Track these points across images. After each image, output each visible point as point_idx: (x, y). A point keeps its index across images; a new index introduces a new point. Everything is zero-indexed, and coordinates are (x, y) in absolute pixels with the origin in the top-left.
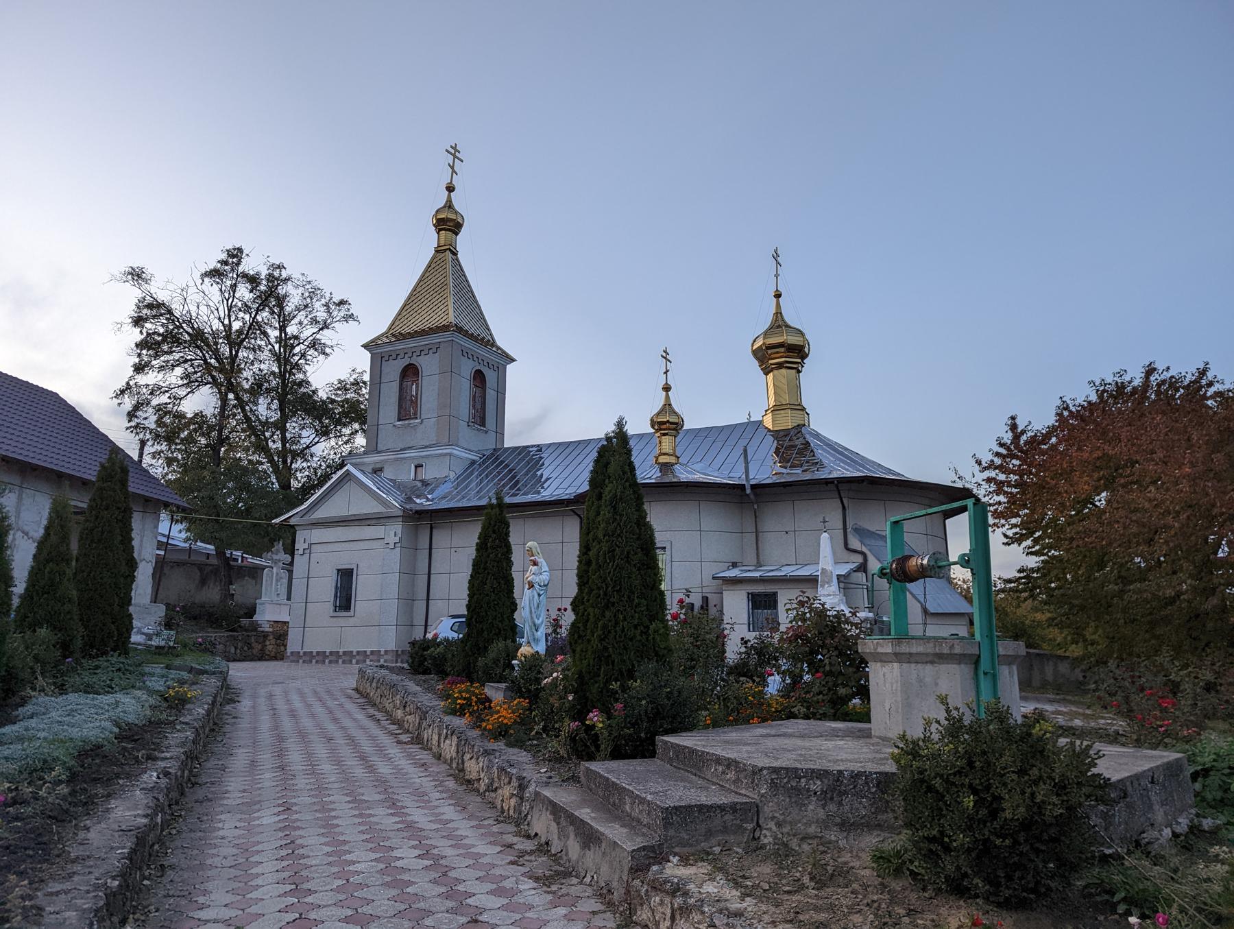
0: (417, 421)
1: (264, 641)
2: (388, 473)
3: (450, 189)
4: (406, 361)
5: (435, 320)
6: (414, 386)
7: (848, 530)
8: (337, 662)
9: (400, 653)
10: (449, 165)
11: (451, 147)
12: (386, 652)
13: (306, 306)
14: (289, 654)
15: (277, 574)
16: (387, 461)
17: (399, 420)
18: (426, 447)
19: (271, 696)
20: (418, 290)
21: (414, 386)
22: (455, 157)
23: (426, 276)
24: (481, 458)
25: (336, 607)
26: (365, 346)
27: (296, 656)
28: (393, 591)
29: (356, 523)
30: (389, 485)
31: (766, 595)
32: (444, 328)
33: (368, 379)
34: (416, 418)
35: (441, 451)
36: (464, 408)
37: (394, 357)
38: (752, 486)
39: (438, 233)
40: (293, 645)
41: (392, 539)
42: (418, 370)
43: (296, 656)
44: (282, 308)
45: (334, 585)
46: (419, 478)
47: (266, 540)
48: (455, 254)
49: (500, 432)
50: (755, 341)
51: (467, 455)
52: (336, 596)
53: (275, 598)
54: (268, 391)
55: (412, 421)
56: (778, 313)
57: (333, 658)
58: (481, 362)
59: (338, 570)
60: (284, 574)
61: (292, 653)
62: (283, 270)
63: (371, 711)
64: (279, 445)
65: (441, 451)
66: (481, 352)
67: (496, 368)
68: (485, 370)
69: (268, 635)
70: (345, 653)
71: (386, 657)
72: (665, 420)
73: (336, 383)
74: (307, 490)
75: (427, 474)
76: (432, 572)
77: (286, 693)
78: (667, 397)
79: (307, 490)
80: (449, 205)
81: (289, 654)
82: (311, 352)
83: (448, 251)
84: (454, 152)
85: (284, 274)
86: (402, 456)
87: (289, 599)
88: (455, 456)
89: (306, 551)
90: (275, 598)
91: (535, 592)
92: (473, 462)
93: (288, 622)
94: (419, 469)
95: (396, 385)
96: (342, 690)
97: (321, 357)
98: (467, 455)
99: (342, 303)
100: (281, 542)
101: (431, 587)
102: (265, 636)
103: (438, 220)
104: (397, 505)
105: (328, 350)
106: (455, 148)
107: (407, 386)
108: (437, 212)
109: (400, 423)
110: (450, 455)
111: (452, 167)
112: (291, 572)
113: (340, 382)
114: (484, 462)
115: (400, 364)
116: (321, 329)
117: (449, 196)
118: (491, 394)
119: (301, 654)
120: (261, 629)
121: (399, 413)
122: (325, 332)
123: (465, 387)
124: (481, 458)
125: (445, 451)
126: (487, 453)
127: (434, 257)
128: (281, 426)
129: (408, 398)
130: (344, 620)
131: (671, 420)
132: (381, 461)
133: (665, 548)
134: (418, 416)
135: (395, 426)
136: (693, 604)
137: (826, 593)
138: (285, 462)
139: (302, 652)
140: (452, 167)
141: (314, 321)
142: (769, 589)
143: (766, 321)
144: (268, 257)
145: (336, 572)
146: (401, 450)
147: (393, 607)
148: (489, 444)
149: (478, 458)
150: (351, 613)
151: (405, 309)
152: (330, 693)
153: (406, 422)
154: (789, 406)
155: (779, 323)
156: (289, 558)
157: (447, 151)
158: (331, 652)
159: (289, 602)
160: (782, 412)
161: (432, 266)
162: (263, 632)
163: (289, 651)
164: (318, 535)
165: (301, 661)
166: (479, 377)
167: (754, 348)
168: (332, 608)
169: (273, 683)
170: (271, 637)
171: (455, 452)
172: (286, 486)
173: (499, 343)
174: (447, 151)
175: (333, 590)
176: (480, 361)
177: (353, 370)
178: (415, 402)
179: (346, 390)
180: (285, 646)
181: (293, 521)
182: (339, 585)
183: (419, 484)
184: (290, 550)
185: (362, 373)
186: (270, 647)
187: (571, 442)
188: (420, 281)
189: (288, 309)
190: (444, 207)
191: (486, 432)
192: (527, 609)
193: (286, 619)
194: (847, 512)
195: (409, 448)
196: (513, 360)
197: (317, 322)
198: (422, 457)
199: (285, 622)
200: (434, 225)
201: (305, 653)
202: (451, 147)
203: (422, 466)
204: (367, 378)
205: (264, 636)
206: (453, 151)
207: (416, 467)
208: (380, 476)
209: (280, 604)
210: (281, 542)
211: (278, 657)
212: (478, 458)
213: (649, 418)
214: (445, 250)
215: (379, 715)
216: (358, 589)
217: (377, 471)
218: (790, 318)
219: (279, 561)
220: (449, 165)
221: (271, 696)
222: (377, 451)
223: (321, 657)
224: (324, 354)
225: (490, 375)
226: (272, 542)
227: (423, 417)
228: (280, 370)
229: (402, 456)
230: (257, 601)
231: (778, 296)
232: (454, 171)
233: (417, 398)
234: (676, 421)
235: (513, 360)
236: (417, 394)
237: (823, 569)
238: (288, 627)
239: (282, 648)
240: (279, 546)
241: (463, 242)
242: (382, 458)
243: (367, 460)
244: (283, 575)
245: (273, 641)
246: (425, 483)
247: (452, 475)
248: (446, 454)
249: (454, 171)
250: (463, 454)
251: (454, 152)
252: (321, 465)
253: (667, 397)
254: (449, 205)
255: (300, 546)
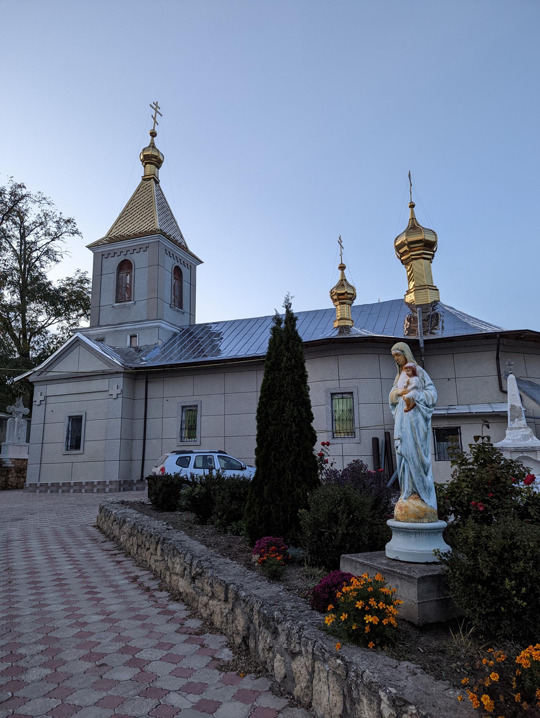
0: (131, 302)
1: (7, 475)
2: (109, 341)
3: (153, 134)
4: (122, 258)
5: (144, 227)
6: (128, 277)
7: (502, 376)
8: (69, 491)
9: (122, 483)
10: (152, 116)
11: (154, 103)
12: (111, 482)
13: (41, 224)
14: (27, 486)
15: (18, 422)
16: (107, 333)
17: (117, 302)
18: (139, 322)
19: (9, 541)
20: (130, 207)
21: (128, 277)
22: (157, 112)
23: (136, 197)
24: (181, 331)
25: (67, 446)
26: (89, 247)
27: (34, 487)
28: (117, 433)
29: (84, 379)
30: (110, 350)
31: (80, 446)
32: (153, 233)
33: (91, 277)
34: (131, 301)
35: (151, 324)
36: (167, 294)
37: (112, 255)
38: (424, 340)
39: (144, 167)
40: (31, 478)
41: (115, 391)
42: (131, 264)
43: (34, 487)
44: (22, 222)
45: (66, 428)
46: (134, 345)
47: (10, 395)
48: (157, 182)
49: (192, 314)
50: (396, 239)
51: (171, 329)
52: (67, 438)
53: (16, 441)
54: (11, 283)
55: (127, 303)
56: (413, 219)
57: (66, 488)
58: (179, 261)
59: (70, 417)
60: (24, 422)
61: (30, 484)
62: (23, 189)
63: (128, 564)
64: (20, 325)
65: (151, 324)
66: (180, 253)
67: (189, 267)
68: (182, 267)
69: (11, 470)
70: (75, 484)
71: (110, 487)
72: (344, 291)
73: (65, 279)
74: (40, 360)
75: (140, 342)
76: (143, 420)
77: (25, 538)
78: (343, 274)
79: (40, 360)
80: (152, 146)
81: (27, 486)
82: (44, 258)
83: (152, 180)
84: (156, 107)
85: (24, 192)
86: (120, 328)
87: (28, 441)
88: (163, 328)
89: (42, 403)
90: (16, 441)
91: (419, 416)
92: (175, 334)
93: (27, 459)
94: (133, 339)
95: (114, 276)
96: (83, 527)
97: (53, 263)
98: (171, 329)
99: (68, 221)
100: (22, 398)
101: (147, 429)
102: (8, 470)
103: (145, 156)
104: (119, 364)
105: (58, 257)
106: (156, 104)
107: (122, 277)
108: (144, 150)
109: (118, 304)
110: (159, 327)
111: (154, 119)
112: (29, 422)
113: (69, 279)
114: (183, 335)
115: (116, 261)
116: (53, 240)
117: (152, 140)
118: (186, 286)
119: (38, 485)
120: (5, 465)
121: (117, 297)
122: (57, 242)
123: (168, 278)
124: (181, 331)
125: (154, 324)
126: (186, 328)
127: (141, 184)
128: (22, 309)
129: (124, 285)
130: (75, 456)
131: (348, 292)
132: (103, 333)
133: (352, 393)
134: (132, 299)
135: (113, 307)
136: (378, 439)
137: (517, 426)
138: (25, 337)
139: (38, 483)
140: (154, 119)
141: (47, 234)
142: (452, 424)
143: (405, 224)
144: (12, 177)
145: (67, 418)
146: (119, 324)
147: (116, 445)
148: (185, 323)
149: (179, 331)
150: (81, 451)
151: (120, 220)
152: (71, 533)
153: (123, 304)
154: (427, 287)
155: (414, 227)
156: (27, 410)
157: (151, 105)
158: (64, 484)
159: (28, 444)
160: (423, 291)
161: (141, 190)
162: (6, 467)
163: (27, 483)
164: (52, 389)
165: (38, 491)
166: (177, 272)
167: (397, 244)
168: (65, 447)
169: (13, 520)
170: (13, 471)
171: (162, 325)
172: (25, 354)
173: (191, 249)
174: (151, 105)
175: (65, 433)
176: (178, 260)
177: (78, 271)
178: (129, 289)
179: (73, 285)
180: (25, 478)
181: (31, 379)
182: (70, 429)
183: (133, 350)
184: (29, 404)
185: (84, 273)
186: (12, 479)
187: (251, 319)
188: (131, 200)
189: (26, 224)
190: (149, 147)
191: (183, 313)
192: (410, 442)
193: (26, 457)
194: (500, 361)
195: (122, 324)
196: (201, 262)
197: (50, 235)
198: (136, 329)
199: (24, 460)
200: (141, 160)
201: (41, 485)
202: (154, 103)
203: (136, 336)
204: (90, 276)
205: (7, 471)
206: (155, 107)
207: (131, 337)
208: (103, 343)
209: (21, 446)
210: (22, 398)
211: (19, 486)
212: (179, 331)
213: (329, 291)
214: (150, 179)
215: (145, 577)
216: (86, 432)
217: (100, 340)
218: (422, 222)
219: (20, 412)
220: (152, 116)
221: (9, 541)
222: (99, 326)
223: (55, 488)
224: (55, 260)
225: (185, 272)
226: (14, 397)
227: (136, 300)
228: (21, 267)
229: (120, 328)
230: (2, 443)
231: (412, 206)
232: (156, 122)
233: (130, 286)
234: (352, 292)
235: (201, 262)
236: (130, 282)
237: (512, 406)
238: (27, 463)
239: (22, 480)
240: (20, 401)
241: (162, 173)
242: (101, 331)
243: (91, 332)
244: (24, 423)
245: (15, 475)
246: (138, 350)
247: (160, 343)
248: (156, 327)
249: (156, 122)
250: (168, 327)
251: (156, 107)
252: (53, 341)
253: (343, 274)
254: (152, 146)
255: (37, 398)
